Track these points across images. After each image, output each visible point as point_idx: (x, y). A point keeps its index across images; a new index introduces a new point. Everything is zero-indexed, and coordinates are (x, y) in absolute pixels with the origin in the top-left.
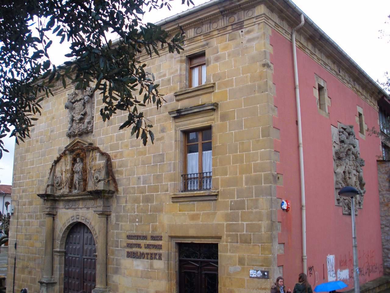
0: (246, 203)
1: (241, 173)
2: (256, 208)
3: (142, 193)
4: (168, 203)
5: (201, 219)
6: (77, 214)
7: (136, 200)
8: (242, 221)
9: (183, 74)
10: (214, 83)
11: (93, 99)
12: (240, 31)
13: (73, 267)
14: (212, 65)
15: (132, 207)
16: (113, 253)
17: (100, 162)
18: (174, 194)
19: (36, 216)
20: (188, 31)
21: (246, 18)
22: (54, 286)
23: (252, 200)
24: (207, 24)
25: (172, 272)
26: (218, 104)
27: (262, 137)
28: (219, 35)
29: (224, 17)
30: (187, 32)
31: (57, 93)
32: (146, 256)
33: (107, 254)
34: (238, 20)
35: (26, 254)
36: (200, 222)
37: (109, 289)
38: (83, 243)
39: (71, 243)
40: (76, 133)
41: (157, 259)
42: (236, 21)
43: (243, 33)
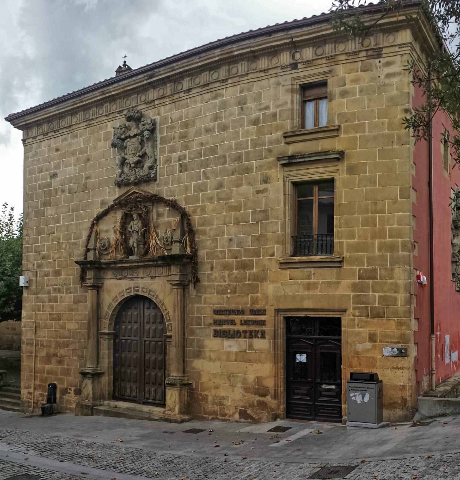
0: (379, 272)
1: (374, 236)
2: (391, 278)
3: (237, 258)
4: (274, 270)
5: (319, 288)
6: (136, 285)
7: (226, 267)
8: (374, 291)
9: (295, 109)
10: (339, 124)
11: (155, 135)
12: (377, 61)
13: (127, 353)
14: (336, 101)
15: (221, 275)
16: (192, 332)
17: (169, 219)
18: (284, 260)
19: (68, 289)
20: (304, 50)
21: (386, 44)
22: (100, 377)
23: (386, 269)
24: (332, 43)
25: (279, 352)
26: (344, 153)
27: (400, 198)
28: (347, 61)
29: (355, 37)
30: (301, 50)
31: (93, 125)
32: (243, 334)
33: (184, 334)
34: (374, 46)
35: (53, 338)
36: (317, 292)
37: (188, 378)
38: (144, 323)
39: (124, 322)
40: (130, 181)
41: (258, 338)
42: (372, 46)
43: (381, 64)
